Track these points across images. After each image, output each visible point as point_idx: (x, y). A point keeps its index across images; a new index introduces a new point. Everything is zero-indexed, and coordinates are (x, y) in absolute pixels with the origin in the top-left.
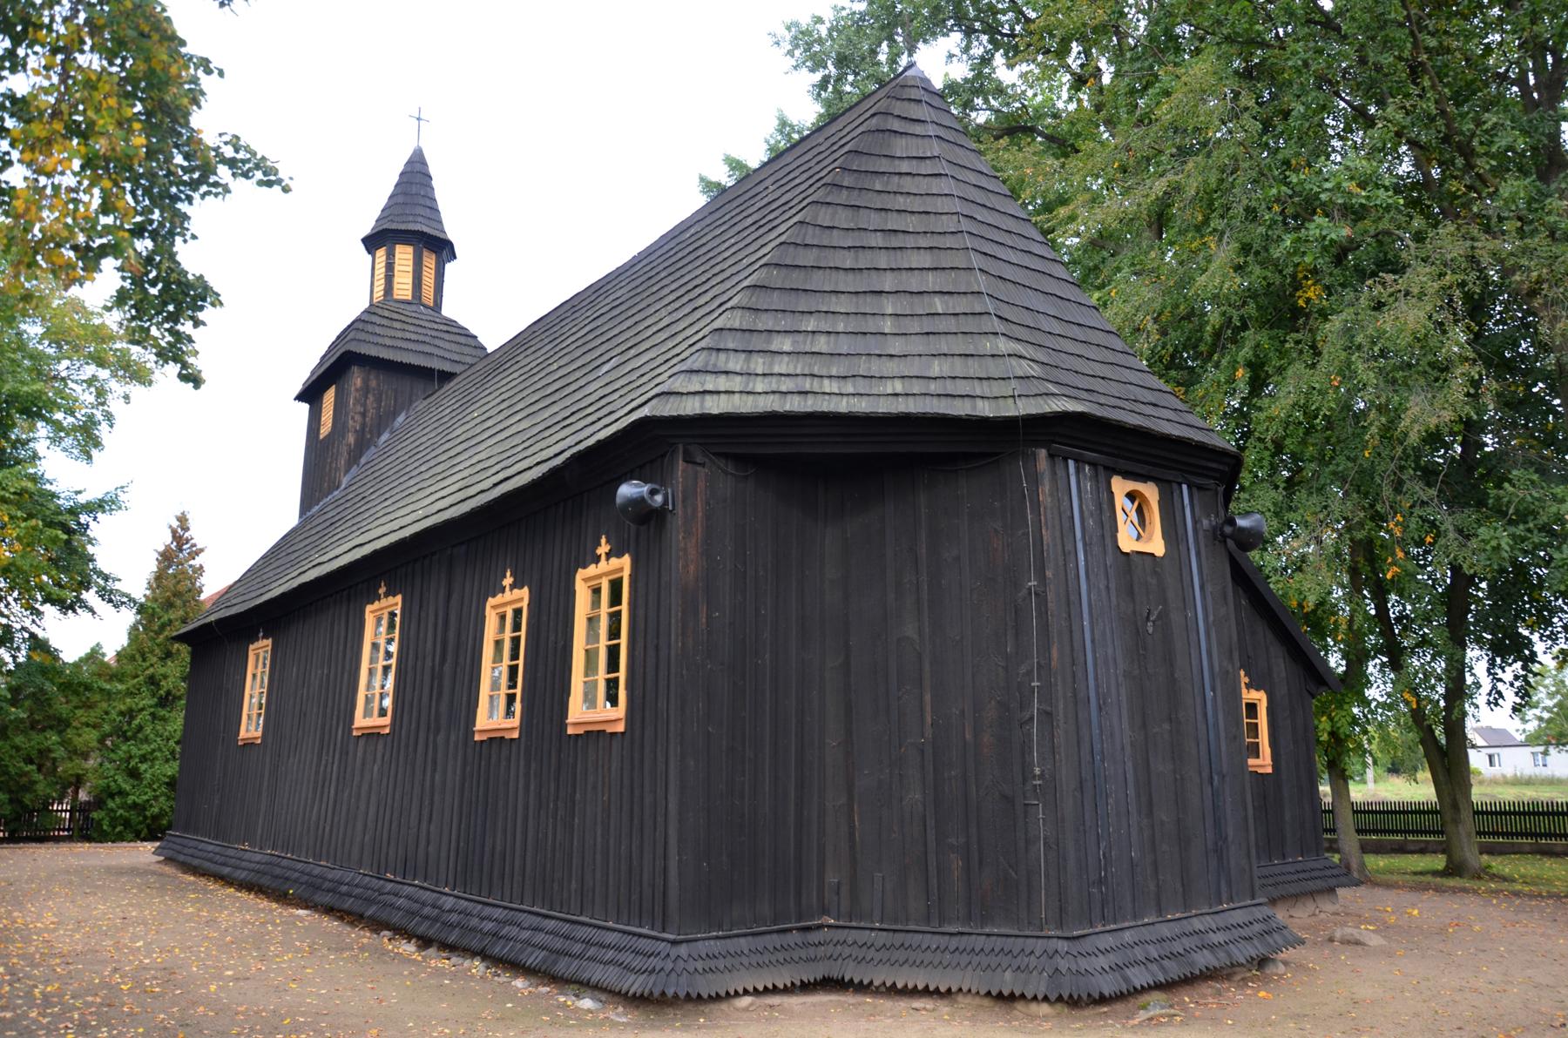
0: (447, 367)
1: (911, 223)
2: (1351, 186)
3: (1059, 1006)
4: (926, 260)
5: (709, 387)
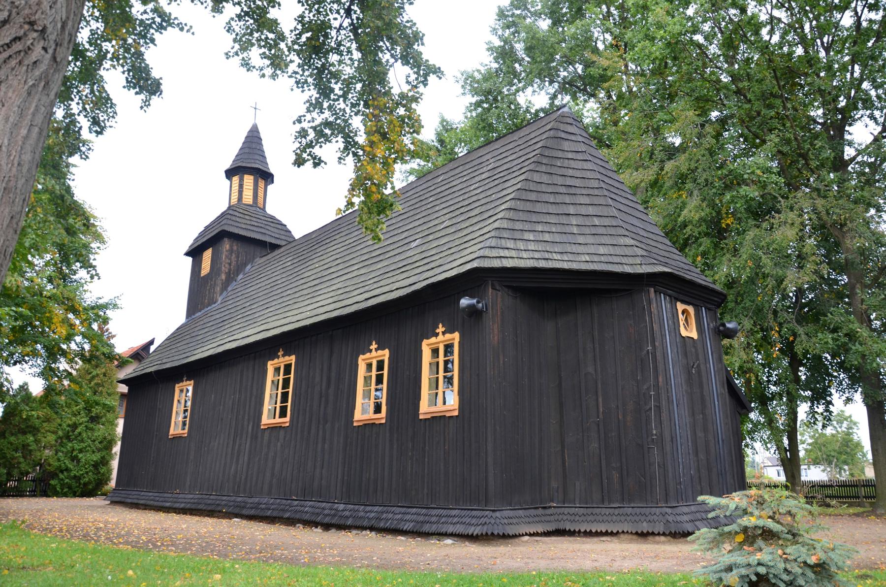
0: (273, 241)
1: (577, 183)
2: (758, 172)
3: (669, 538)
4: (586, 200)
5: (502, 255)
